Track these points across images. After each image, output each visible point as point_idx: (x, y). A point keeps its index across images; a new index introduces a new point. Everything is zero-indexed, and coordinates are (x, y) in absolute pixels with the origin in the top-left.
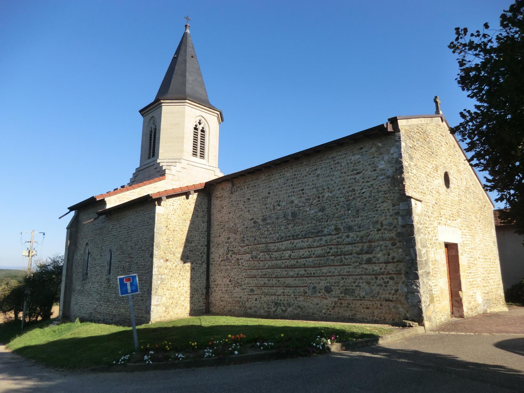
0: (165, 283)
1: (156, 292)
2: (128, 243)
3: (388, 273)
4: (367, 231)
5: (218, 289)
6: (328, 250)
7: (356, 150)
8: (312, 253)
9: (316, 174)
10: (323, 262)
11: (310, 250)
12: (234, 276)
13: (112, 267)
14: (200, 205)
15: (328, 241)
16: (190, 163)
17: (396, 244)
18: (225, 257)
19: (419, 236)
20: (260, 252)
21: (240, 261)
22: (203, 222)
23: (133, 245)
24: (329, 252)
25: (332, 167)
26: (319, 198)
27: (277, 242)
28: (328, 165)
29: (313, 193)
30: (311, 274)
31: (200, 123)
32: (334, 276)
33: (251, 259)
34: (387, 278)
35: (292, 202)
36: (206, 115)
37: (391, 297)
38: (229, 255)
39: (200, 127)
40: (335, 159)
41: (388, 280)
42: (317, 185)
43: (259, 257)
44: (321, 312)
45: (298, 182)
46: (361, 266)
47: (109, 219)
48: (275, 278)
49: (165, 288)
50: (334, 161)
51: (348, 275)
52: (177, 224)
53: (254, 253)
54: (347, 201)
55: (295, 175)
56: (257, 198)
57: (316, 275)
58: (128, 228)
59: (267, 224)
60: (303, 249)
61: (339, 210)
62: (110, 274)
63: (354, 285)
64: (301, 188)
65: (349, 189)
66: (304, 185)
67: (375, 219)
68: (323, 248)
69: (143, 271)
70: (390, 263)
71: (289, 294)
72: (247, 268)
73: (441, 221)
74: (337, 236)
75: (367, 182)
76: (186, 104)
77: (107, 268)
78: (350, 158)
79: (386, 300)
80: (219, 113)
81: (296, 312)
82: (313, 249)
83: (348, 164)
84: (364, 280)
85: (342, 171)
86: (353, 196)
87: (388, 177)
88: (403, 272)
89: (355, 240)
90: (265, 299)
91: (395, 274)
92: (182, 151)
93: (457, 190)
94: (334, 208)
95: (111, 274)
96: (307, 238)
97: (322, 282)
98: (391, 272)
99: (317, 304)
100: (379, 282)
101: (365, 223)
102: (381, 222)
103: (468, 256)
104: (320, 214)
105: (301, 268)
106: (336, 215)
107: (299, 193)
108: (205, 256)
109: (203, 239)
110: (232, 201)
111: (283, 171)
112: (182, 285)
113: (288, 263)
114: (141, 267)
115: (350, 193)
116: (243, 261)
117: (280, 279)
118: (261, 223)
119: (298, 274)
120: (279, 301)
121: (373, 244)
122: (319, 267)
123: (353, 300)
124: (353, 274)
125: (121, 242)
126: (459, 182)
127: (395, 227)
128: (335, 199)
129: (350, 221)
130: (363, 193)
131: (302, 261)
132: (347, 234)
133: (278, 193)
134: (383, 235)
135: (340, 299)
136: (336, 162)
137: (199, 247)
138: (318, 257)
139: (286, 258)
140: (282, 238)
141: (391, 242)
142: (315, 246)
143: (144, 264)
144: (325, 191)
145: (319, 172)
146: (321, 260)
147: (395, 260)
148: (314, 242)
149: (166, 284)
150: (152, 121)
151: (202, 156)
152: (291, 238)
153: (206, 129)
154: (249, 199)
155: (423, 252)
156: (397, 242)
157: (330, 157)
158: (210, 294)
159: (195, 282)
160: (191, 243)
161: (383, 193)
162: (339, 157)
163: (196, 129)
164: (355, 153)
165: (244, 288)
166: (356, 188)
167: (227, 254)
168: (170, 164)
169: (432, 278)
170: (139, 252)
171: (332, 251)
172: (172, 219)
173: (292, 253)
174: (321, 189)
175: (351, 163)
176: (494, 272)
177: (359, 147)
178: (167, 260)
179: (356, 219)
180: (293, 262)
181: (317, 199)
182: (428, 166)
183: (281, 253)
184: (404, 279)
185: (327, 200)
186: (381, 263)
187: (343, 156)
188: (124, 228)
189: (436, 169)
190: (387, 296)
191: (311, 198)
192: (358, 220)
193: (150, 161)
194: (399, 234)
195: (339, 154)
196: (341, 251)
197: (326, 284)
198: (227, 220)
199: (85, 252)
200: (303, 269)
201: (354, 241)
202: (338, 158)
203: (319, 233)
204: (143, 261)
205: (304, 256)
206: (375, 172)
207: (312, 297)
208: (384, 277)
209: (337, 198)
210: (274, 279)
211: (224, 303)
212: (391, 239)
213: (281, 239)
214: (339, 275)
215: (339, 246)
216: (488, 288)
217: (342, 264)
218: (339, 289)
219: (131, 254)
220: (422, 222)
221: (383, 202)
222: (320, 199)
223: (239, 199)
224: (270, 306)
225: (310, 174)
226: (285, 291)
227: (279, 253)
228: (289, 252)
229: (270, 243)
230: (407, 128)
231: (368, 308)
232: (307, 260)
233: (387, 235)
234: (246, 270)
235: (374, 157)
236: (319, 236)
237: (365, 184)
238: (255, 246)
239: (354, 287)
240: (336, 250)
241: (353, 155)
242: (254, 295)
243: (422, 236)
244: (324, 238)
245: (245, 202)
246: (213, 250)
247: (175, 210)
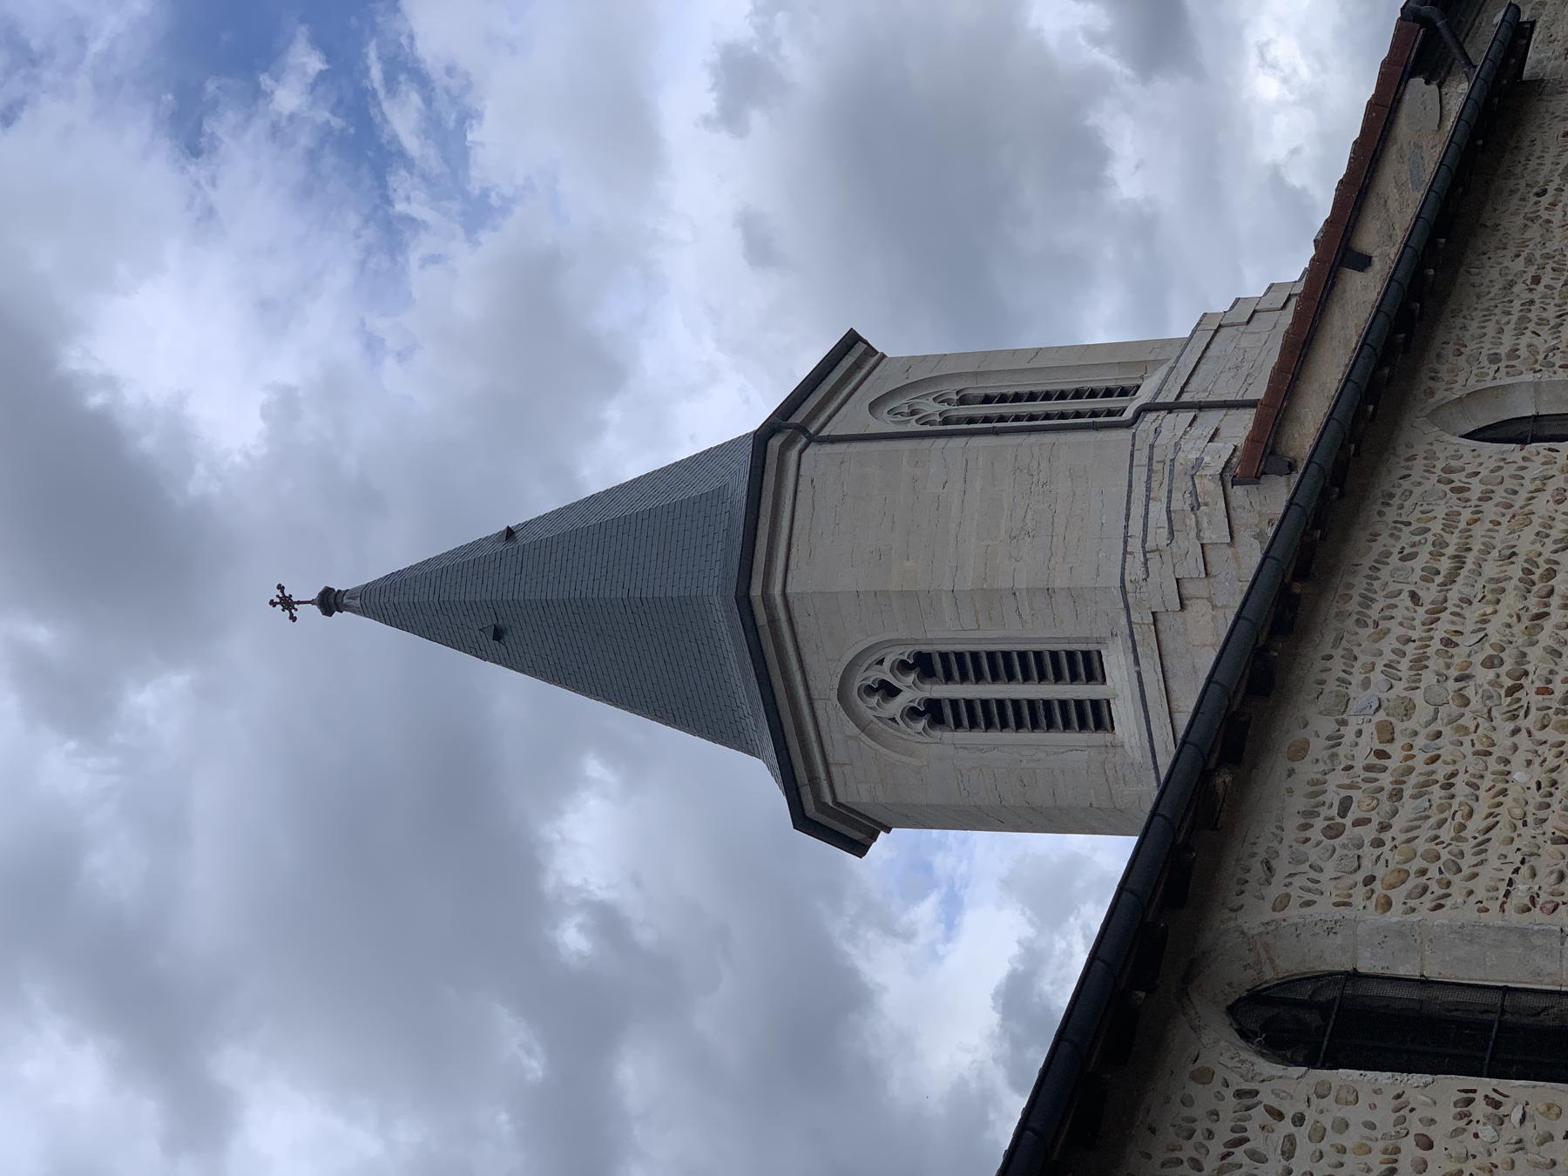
39: (913, 691)
153: (906, 652)
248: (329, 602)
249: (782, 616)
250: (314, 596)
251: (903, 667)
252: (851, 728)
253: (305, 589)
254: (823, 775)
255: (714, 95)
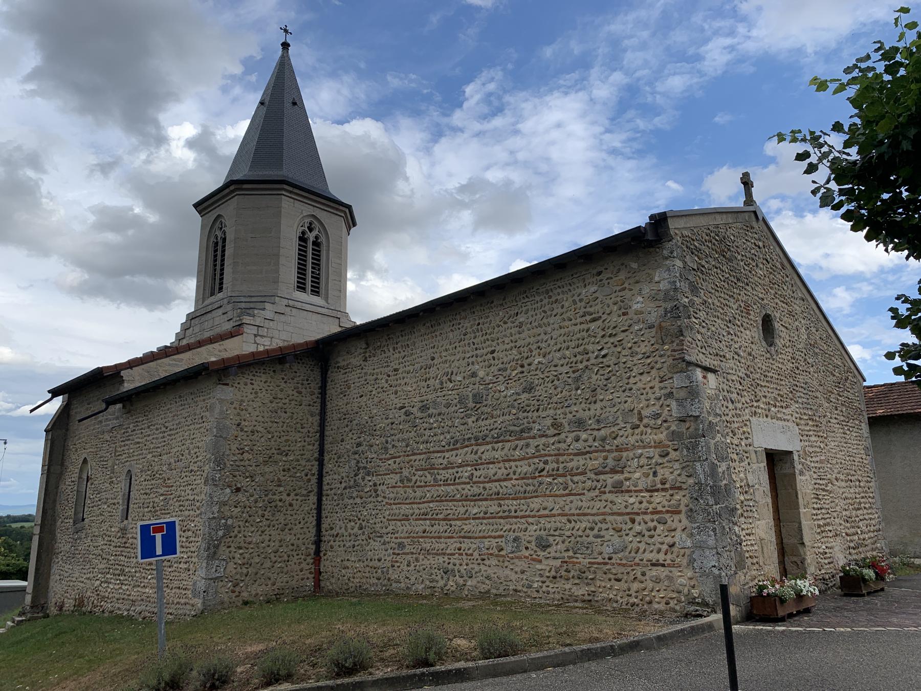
0: (232, 534)
2: (164, 457)
3: (655, 512)
4: (613, 429)
5: (337, 543)
6: (541, 465)
7: (589, 276)
8: (511, 471)
9: (517, 323)
10: (531, 488)
11: (507, 465)
12: (368, 517)
13: (131, 506)
14: (305, 382)
15: (541, 447)
16: (291, 303)
17: (667, 454)
18: (352, 480)
19: (713, 438)
20: (417, 470)
21: (380, 488)
22: (312, 416)
23: (172, 460)
24: (543, 470)
25: (547, 308)
26: (522, 366)
27: (448, 451)
28: (539, 305)
29: (512, 357)
30: (510, 511)
32: (554, 516)
33: (399, 484)
34: (652, 521)
35: (474, 375)
37: (661, 557)
38: (360, 476)
39: (311, 236)
40: (551, 294)
41: (655, 523)
42: (518, 344)
43: (414, 479)
44: (530, 587)
45: (485, 337)
46: (604, 497)
47: (129, 412)
48: (444, 520)
49: (232, 545)
50: (550, 297)
51: (578, 515)
52: (260, 419)
53: (406, 473)
54: (574, 372)
55: (479, 324)
56: (411, 368)
57: (519, 514)
58: (164, 429)
59: (430, 416)
60: (494, 463)
61: (559, 389)
62: (127, 519)
63: (592, 533)
64: (490, 349)
65: (576, 350)
66: (494, 344)
67: (626, 405)
68: (530, 461)
69: (192, 513)
70: (657, 490)
71: (470, 552)
72: (392, 501)
73: (757, 410)
74: (556, 438)
75: (610, 336)
77: (121, 508)
78: (578, 291)
79: (653, 565)
80: (347, 211)
81: (483, 588)
82: (513, 464)
83: (574, 302)
84: (609, 525)
85: (565, 316)
86: (585, 363)
87: (651, 327)
88: (683, 508)
89: (590, 447)
90: (426, 562)
91: (668, 512)
92: (276, 281)
93: (790, 350)
94: (550, 385)
95: (129, 518)
96: (502, 441)
97: (530, 528)
98: (660, 508)
99: (523, 572)
100: (638, 528)
101: (607, 414)
102: (639, 413)
103: (815, 476)
104: (524, 396)
105: (492, 500)
106: (555, 399)
107: (486, 358)
108: (314, 480)
109: (311, 447)
110: (366, 373)
111: (458, 317)
112: (267, 538)
113: (468, 490)
114: (187, 503)
115: (579, 358)
116: (384, 487)
117: (453, 523)
118: (419, 415)
119: (486, 513)
120: (451, 567)
121: (625, 454)
122: (525, 498)
123: (590, 563)
124: (589, 511)
125: (149, 456)
126: (792, 335)
127: (665, 421)
128: (553, 368)
129: (579, 410)
130: (604, 356)
131: (494, 487)
132: (575, 433)
133: (449, 358)
134: (644, 437)
135: (566, 562)
136: (553, 299)
137: (303, 463)
138: (523, 478)
139: (464, 480)
140: (457, 442)
141: (658, 450)
142: (517, 457)
143: (192, 498)
144: (533, 354)
145: (521, 318)
146: (528, 485)
147: (667, 486)
148: (514, 449)
149: (236, 536)
150: (218, 224)
151: (316, 291)
152: (473, 442)
154: (396, 370)
155: (720, 470)
156: (670, 450)
157: (541, 291)
158: (322, 554)
159: (293, 532)
160: (287, 455)
161: (640, 356)
162: (559, 290)
163: (303, 239)
164: (587, 282)
165: (387, 540)
166: (590, 347)
167: (356, 475)
168: (252, 305)
169: (742, 519)
170: (184, 475)
171: (547, 467)
173: (474, 472)
174: (526, 349)
175: (581, 300)
176: (867, 506)
177: (595, 272)
178: (238, 490)
179: (592, 406)
180: (476, 490)
181: (520, 369)
182: (731, 304)
183: (454, 471)
184: (685, 522)
185: (536, 370)
186: (641, 491)
187: (566, 289)
188: (157, 429)
189: (747, 309)
190: (653, 556)
191: (508, 366)
192: (596, 409)
193: (212, 299)
194: (674, 436)
195: (559, 284)
196: (565, 467)
197: (538, 532)
198: (356, 409)
199: (80, 478)
200: (496, 502)
201: (588, 449)
202: (555, 292)
203: (523, 433)
204: (190, 492)
205: (496, 477)
206: (625, 317)
207: (512, 558)
208: (647, 518)
209: (555, 366)
210: (441, 522)
211: (348, 573)
212: (659, 444)
213: (455, 445)
214: (562, 515)
215: (561, 459)
216: (856, 537)
217: (567, 492)
218: (563, 542)
219: (169, 479)
220: (718, 411)
221: (641, 374)
222: (524, 369)
223: (378, 371)
224: (433, 576)
225: (505, 323)
226: (463, 546)
227: (450, 471)
228: (469, 469)
229: (434, 452)
230: (686, 233)
231: (618, 580)
232: (503, 484)
233: (652, 437)
234: (391, 504)
235: (624, 289)
236: (524, 439)
237: (607, 339)
238: (407, 459)
239: (591, 539)
240: (556, 466)
241: (585, 286)
242: (404, 554)
243: (717, 439)
244: (533, 443)
245: (389, 376)
246: (328, 466)
247: (256, 393)
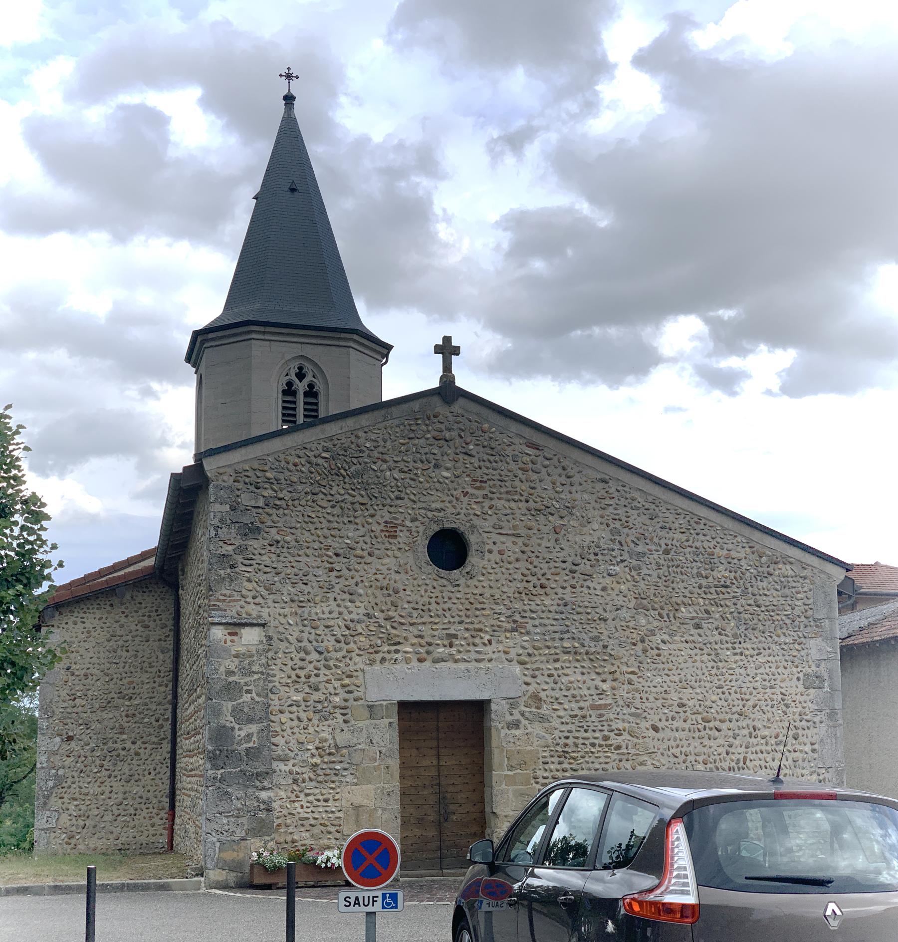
1: (45, 804)
31: (301, 376)
36: (310, 351)
39: (301, 387)
52: (94, 660)
76: (254, 336)
108: (168, 726)
109: (163, 689)
149: (70, 787)
153: (319, 387)
163: (289, 391)
172: (82, 651)
178: (70, 738)
248: (289, 99)
249: (341, 343)
250: (293, 92)
251: (311, 386)
252: (288, 357)
253: (296, 88)
254: (267, 338)
255: (513, 380)
